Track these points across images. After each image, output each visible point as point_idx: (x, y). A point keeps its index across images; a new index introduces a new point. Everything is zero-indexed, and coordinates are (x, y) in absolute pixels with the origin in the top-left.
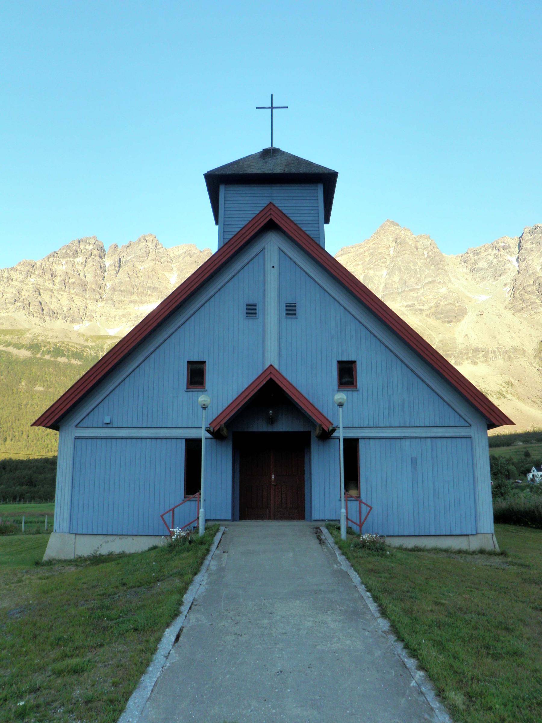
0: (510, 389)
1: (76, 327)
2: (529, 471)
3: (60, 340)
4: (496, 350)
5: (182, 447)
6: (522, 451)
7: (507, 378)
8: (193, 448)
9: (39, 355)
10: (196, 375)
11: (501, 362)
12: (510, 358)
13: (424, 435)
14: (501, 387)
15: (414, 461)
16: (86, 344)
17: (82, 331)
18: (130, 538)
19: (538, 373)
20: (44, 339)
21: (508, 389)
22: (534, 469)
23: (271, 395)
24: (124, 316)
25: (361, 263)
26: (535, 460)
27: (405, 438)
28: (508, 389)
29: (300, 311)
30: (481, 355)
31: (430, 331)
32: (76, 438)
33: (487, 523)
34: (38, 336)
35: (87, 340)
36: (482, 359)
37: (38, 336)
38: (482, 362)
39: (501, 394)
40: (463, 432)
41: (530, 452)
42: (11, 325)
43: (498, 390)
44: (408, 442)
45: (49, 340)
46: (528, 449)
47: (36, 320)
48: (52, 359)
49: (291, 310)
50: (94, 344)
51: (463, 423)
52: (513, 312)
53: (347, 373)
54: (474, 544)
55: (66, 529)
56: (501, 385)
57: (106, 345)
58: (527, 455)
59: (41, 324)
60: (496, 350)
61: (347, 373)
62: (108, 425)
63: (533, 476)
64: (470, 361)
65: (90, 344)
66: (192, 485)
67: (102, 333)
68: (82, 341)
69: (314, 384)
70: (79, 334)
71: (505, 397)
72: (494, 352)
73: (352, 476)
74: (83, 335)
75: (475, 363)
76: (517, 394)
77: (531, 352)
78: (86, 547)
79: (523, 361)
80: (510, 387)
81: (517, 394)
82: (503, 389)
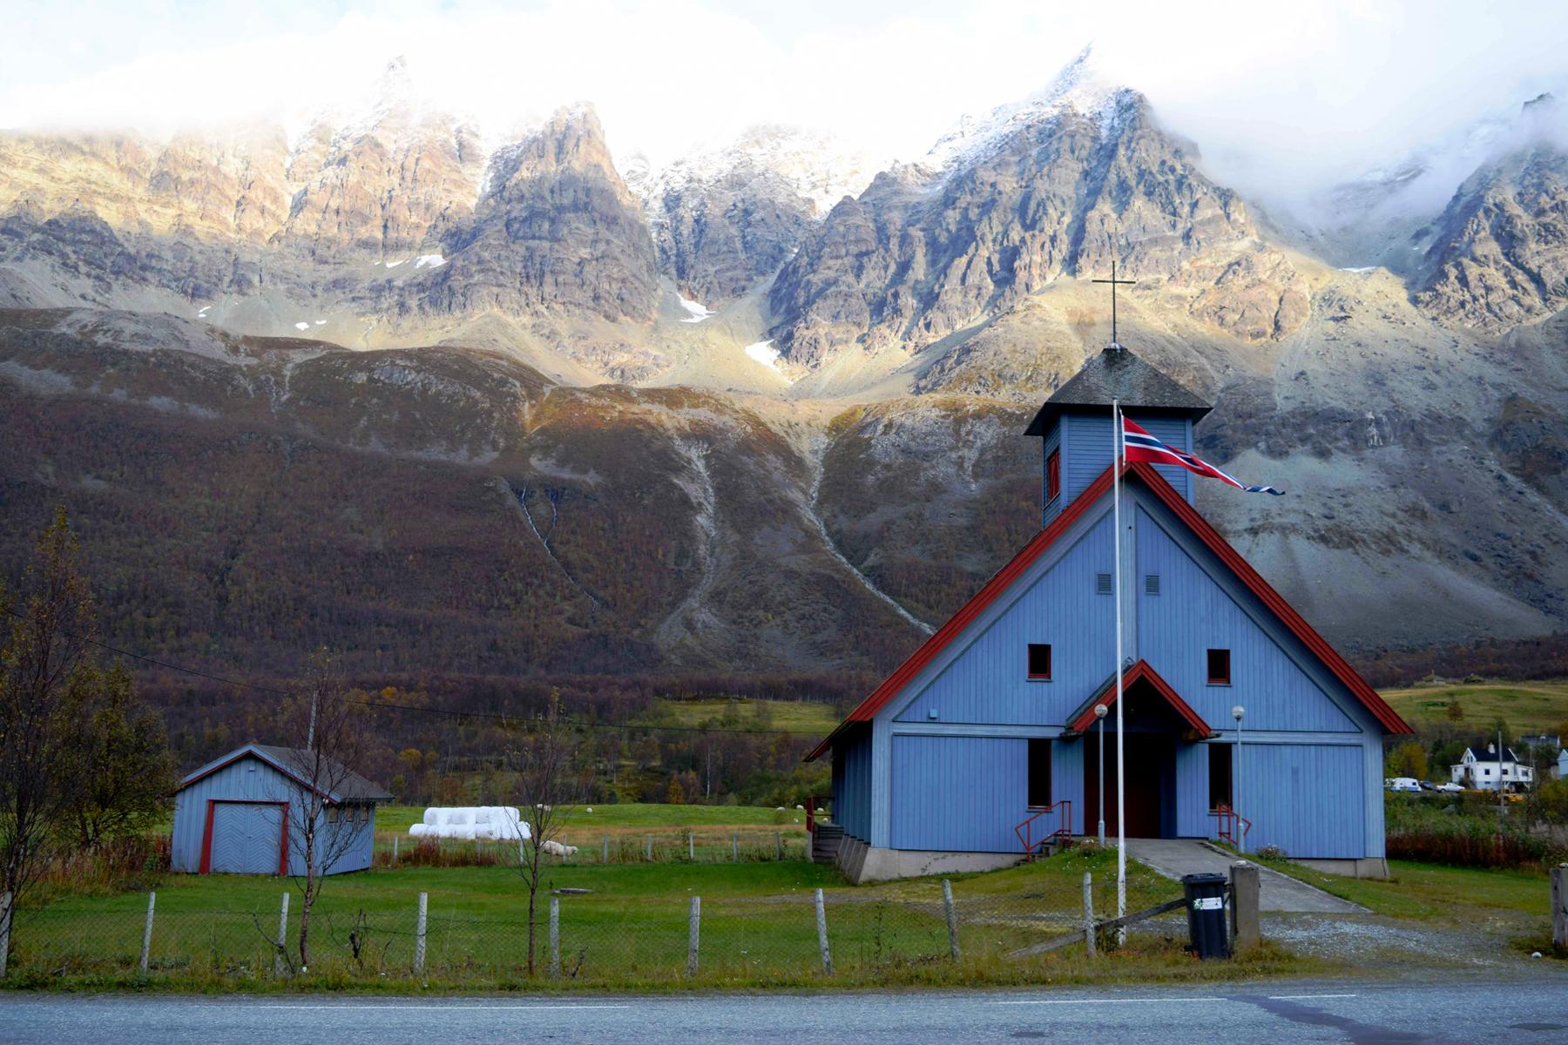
0: (1417, 529)
1: (202, 312)
2: (1457, 760)
3: (158, 346)
4: (1385, 419)
5: (1023, 749)
6: (1443, 704)
7: (1410, 496)
8: (1039, 752)
9: (94, 389)
10: (1040, 661)
11: (1395, 453)
12: (1421, 441)
13: (1307, 741)
14: (1392, 522)
15: (1295, 772)
16: (231, 360)
17: (220, 323)
18: (964, 856)
19: (1496, 485)
20: (110, 340)
21: (1412, 528)
22: (1469, 753)
23: (1146, 693)
24: (336, 284)
25: (1017, 158)
26: (1475, 729)
27: (1286, 744)
28: (1412, 528)
29: (1164, 590)
30: (1340, 431)
31: (1204, 361)
32: (896, 735)
33: (1377, 848)
34: (95, 331)
35: (235, 350)
36: (1346, 442)
37: (95, 331)
38: (1344, 451)
39: (1391, 542)
40: (1354, 739)
41: (1462, 706)
42: (14, 296)
43: (1385, 529)
44: (1287, 750)
45: (127, 346)
46: (1457, 698)
47: (86, 285)
48: (135, 401)
49: (1152, 585)
50: (254, 361)
51: (1354, 728)
52: (1435, 312)
53: (1219, 665)
54: (1363, 869)
55: (887, 844)
56: (1394, 516)
57: (290, 366)
58: (1455, 712)
59: (99, 299)
60: (1385, 419)
61: (1219, 665)
62: (932, 720)
63: (1467, 770)
64: (1308, 447)
65: (243, 361)
66: (1039, 793)
67: (279, 331)
68: (218, 350)
69: (1187, 681)
70: (213, 330)
71: (1402, 550)
72: (1378, 422)
73: (1221, 792)
74: (225, 336)
75: (1323, 454)
76: (1436, 542)
77: (1480, 426)
78: (910, 865)
79: (1457, 451)
80: (1419, 523)
81: (1436, 542)
82: (1399, 528)
